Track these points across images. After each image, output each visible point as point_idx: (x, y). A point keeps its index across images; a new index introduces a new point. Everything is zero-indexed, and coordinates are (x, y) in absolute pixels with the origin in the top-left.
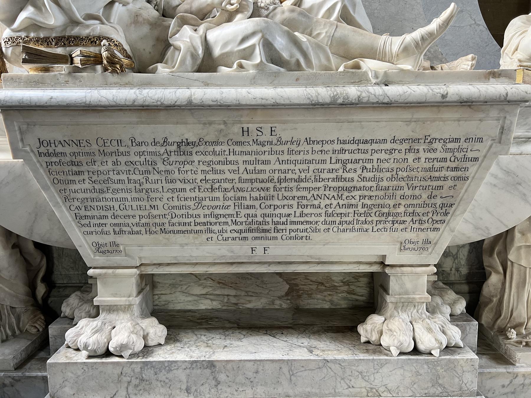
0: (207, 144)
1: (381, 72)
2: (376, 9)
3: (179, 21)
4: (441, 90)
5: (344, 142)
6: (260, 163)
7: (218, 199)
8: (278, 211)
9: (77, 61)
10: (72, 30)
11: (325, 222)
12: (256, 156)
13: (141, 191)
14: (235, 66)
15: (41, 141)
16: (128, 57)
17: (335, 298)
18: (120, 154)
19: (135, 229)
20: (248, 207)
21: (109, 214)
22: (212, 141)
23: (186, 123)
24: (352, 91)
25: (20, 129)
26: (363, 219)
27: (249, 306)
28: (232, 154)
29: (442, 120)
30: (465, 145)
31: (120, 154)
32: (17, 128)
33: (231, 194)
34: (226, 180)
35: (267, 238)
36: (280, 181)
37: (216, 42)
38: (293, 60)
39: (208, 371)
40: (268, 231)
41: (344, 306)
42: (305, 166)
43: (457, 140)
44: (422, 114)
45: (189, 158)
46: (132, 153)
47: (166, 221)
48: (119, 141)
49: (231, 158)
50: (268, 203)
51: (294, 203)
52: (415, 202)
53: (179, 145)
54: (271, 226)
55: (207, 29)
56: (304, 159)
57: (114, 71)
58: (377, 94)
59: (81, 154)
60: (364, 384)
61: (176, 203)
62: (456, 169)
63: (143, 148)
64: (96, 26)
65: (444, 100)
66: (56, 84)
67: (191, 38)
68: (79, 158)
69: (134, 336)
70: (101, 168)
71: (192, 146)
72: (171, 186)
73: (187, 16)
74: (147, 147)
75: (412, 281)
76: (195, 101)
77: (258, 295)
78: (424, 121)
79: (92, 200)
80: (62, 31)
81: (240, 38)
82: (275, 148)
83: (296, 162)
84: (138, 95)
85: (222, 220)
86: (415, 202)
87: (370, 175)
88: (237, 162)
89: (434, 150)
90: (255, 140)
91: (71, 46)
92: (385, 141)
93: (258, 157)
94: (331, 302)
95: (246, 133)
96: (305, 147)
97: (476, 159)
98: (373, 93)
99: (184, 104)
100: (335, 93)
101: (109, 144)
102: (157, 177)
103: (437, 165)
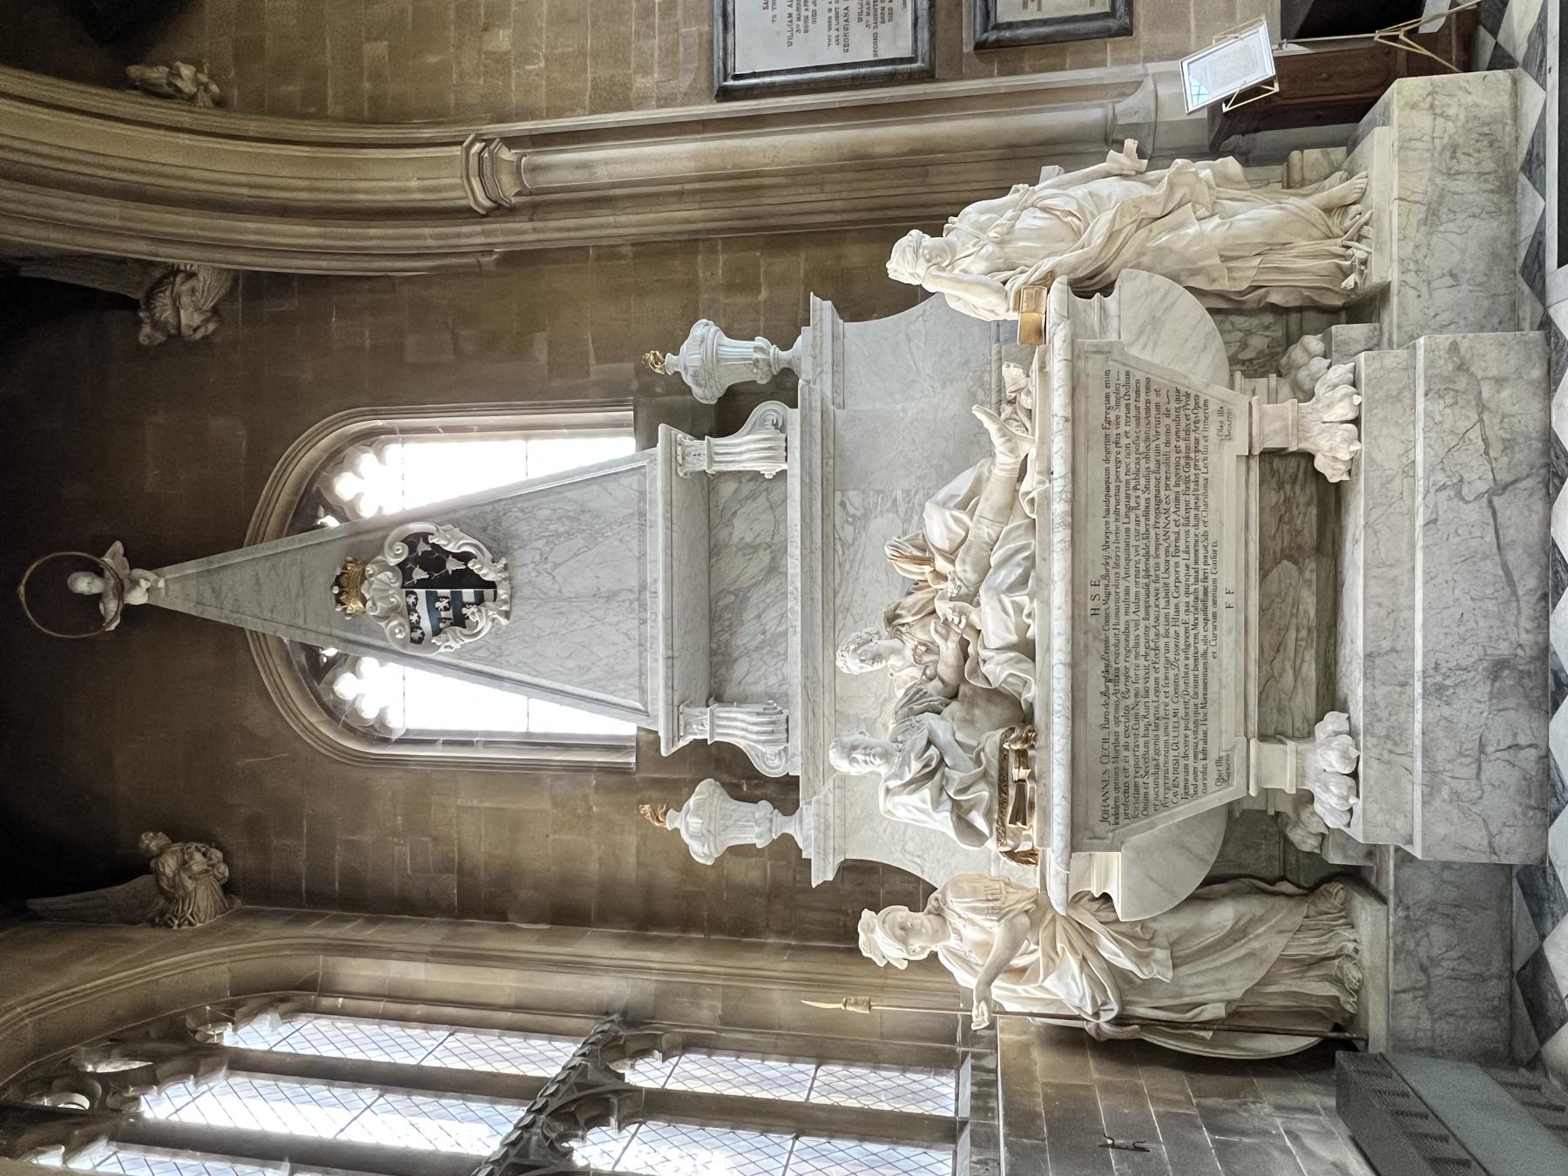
5: (1108, 511)
7: (1167, 644)
8: (1182, 579)
11: (1196, 526)
13: (1157, 725)
14: (1028, 621)
16: (1013, 730)
17: (1302, 500)
19: (1201, 736)
20: (1177, 611)
21: (1182, 762)
24: (1059, 508)
26: (1192, 485)
27: (1312, 613)
29: (1087, 411)
33: (1162, 630)
34: (1146, 634)
35: (1215, 590)
36: (1148, 576)
39: (1378, 661)
40: (1206, 590)
41: (1314, 487)
42: (1132, 550)
43: (1107, 397)
44: (1081, 438)
45: (1122, 671)
47: (1192, 702)
50: (1172, 588)
51: (1172, 561)
52: (1173, 430)
54: (1200, 586)
60: (1397, 482)
61: (1171, 689)
62: (1137, 392)
63: (1111, 718)
66: (1047, 795)
69: (1334, 744)
70: (1132, 762)
72: (1152, 692)
75: (1269, 417)
77: (1296, 602)
79: (1166, 778)
82: (1113, 582)
83: (1128, 560)
85: (1191, 640)
86: (1173, 430)
87: (1143, 481)
89: (1118, 417)
92: (1107, 470)
94: (1309, 504)
97: (1128, 374)
102: (1141, 706)
103: (1133, 413)
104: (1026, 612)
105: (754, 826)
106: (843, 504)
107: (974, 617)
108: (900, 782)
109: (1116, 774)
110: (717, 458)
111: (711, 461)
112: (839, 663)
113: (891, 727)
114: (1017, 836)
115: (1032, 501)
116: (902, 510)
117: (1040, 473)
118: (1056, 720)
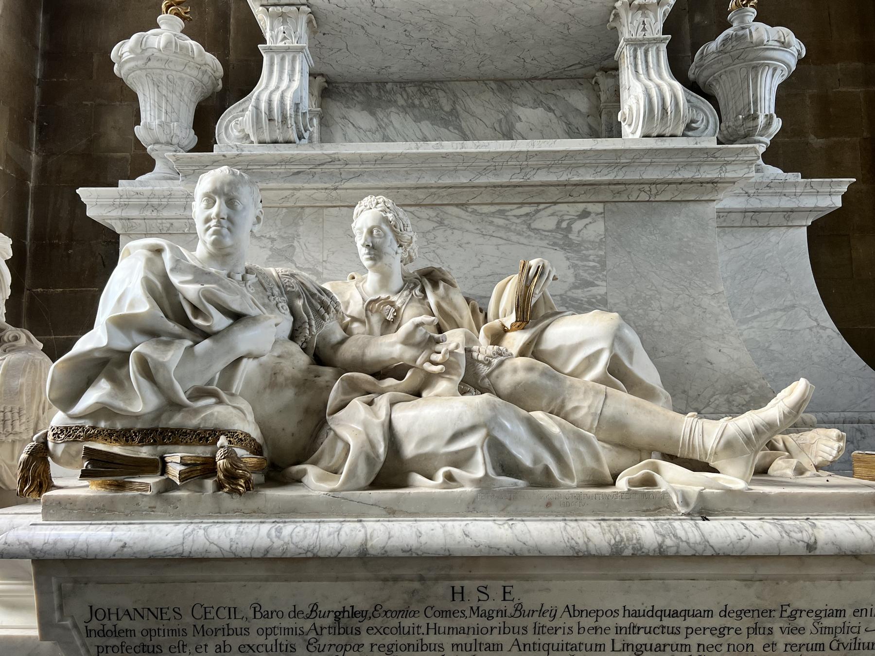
0: (389, 614)
1: (694, 490)
2: (657, 320)
3: (345, 384)
4: (805, 533)
6: (483, 648)
9: (175, 470)
10: (170, 418)
12: (476, 636)
15: (94, 610)
18: (231, 632)
22: (398, 609)
23: (352, 579)
24: (646, 531)
25: (60, 588)
28: (432, 632)
29: (812, 579)
30: (854, 622)
31: (231, 632)
32: (54, 588)
37: (408, 433)
38: (539, 467)
43: (840, 613)
45: (355, 640)
46: (253, 631)
48: (232, 610)
49: (431, 639)
53: (338, 616)
55: (392, 404)
56: (565, 642)
57: (234, 491)
58: (692, 540)
59: (161, 633)
63: (274, 622)
64: (209, 412)
65: (812, 554)
67: (366, 425)
68: (156, 640)
71: (361, 619)
73: (357, 378)
74: (281, 621)
76: (372, 552)
78: (777, 580)
80: (154, 420)
81: (449, 433)
82: (511, 622)
84: (275, 540)
88: (441, 647)
89: (801, 630)
90: (475, 609)
91: (165, 444)
92: (709, 613)
93: (480, 638)
95: (458, 597)
96: (564, 621)
98: (684, 539)
99: (353, 556)
100: (618, 538)
101: (213, 614)
104: (455, 471)
105: (160, 118)
106: (585, 214)
107: (443, 385)
108: (168, 266)
109: (174, 632)
110: (640, 54)
111: (636, 44)
112: (367, 201)
113: (273, 271)
114: (67, 461)
115: (648, 481)
116: (579, 294)
117: (701, 496)
118: (265, 528)
